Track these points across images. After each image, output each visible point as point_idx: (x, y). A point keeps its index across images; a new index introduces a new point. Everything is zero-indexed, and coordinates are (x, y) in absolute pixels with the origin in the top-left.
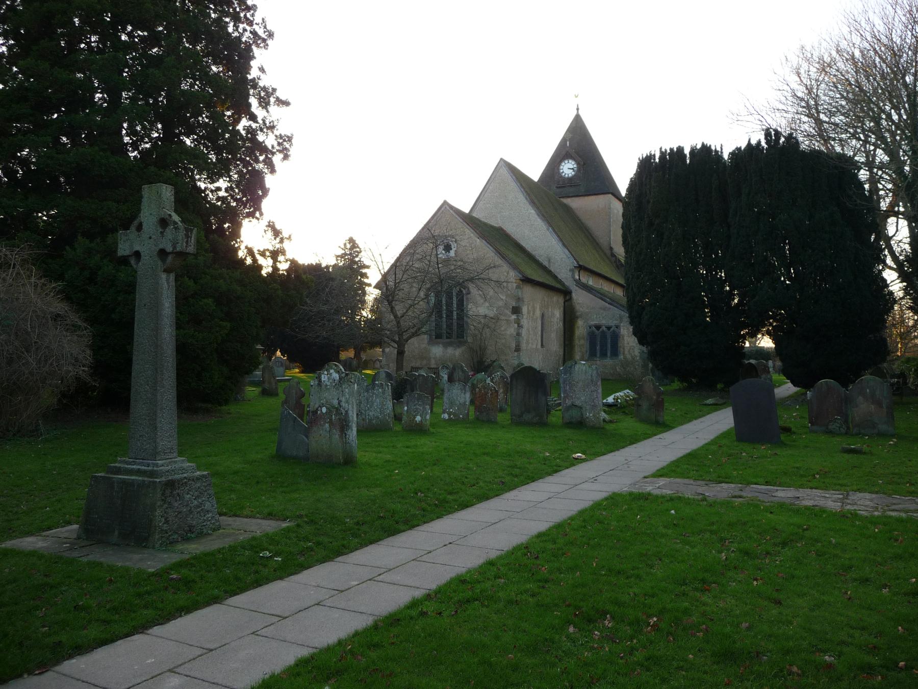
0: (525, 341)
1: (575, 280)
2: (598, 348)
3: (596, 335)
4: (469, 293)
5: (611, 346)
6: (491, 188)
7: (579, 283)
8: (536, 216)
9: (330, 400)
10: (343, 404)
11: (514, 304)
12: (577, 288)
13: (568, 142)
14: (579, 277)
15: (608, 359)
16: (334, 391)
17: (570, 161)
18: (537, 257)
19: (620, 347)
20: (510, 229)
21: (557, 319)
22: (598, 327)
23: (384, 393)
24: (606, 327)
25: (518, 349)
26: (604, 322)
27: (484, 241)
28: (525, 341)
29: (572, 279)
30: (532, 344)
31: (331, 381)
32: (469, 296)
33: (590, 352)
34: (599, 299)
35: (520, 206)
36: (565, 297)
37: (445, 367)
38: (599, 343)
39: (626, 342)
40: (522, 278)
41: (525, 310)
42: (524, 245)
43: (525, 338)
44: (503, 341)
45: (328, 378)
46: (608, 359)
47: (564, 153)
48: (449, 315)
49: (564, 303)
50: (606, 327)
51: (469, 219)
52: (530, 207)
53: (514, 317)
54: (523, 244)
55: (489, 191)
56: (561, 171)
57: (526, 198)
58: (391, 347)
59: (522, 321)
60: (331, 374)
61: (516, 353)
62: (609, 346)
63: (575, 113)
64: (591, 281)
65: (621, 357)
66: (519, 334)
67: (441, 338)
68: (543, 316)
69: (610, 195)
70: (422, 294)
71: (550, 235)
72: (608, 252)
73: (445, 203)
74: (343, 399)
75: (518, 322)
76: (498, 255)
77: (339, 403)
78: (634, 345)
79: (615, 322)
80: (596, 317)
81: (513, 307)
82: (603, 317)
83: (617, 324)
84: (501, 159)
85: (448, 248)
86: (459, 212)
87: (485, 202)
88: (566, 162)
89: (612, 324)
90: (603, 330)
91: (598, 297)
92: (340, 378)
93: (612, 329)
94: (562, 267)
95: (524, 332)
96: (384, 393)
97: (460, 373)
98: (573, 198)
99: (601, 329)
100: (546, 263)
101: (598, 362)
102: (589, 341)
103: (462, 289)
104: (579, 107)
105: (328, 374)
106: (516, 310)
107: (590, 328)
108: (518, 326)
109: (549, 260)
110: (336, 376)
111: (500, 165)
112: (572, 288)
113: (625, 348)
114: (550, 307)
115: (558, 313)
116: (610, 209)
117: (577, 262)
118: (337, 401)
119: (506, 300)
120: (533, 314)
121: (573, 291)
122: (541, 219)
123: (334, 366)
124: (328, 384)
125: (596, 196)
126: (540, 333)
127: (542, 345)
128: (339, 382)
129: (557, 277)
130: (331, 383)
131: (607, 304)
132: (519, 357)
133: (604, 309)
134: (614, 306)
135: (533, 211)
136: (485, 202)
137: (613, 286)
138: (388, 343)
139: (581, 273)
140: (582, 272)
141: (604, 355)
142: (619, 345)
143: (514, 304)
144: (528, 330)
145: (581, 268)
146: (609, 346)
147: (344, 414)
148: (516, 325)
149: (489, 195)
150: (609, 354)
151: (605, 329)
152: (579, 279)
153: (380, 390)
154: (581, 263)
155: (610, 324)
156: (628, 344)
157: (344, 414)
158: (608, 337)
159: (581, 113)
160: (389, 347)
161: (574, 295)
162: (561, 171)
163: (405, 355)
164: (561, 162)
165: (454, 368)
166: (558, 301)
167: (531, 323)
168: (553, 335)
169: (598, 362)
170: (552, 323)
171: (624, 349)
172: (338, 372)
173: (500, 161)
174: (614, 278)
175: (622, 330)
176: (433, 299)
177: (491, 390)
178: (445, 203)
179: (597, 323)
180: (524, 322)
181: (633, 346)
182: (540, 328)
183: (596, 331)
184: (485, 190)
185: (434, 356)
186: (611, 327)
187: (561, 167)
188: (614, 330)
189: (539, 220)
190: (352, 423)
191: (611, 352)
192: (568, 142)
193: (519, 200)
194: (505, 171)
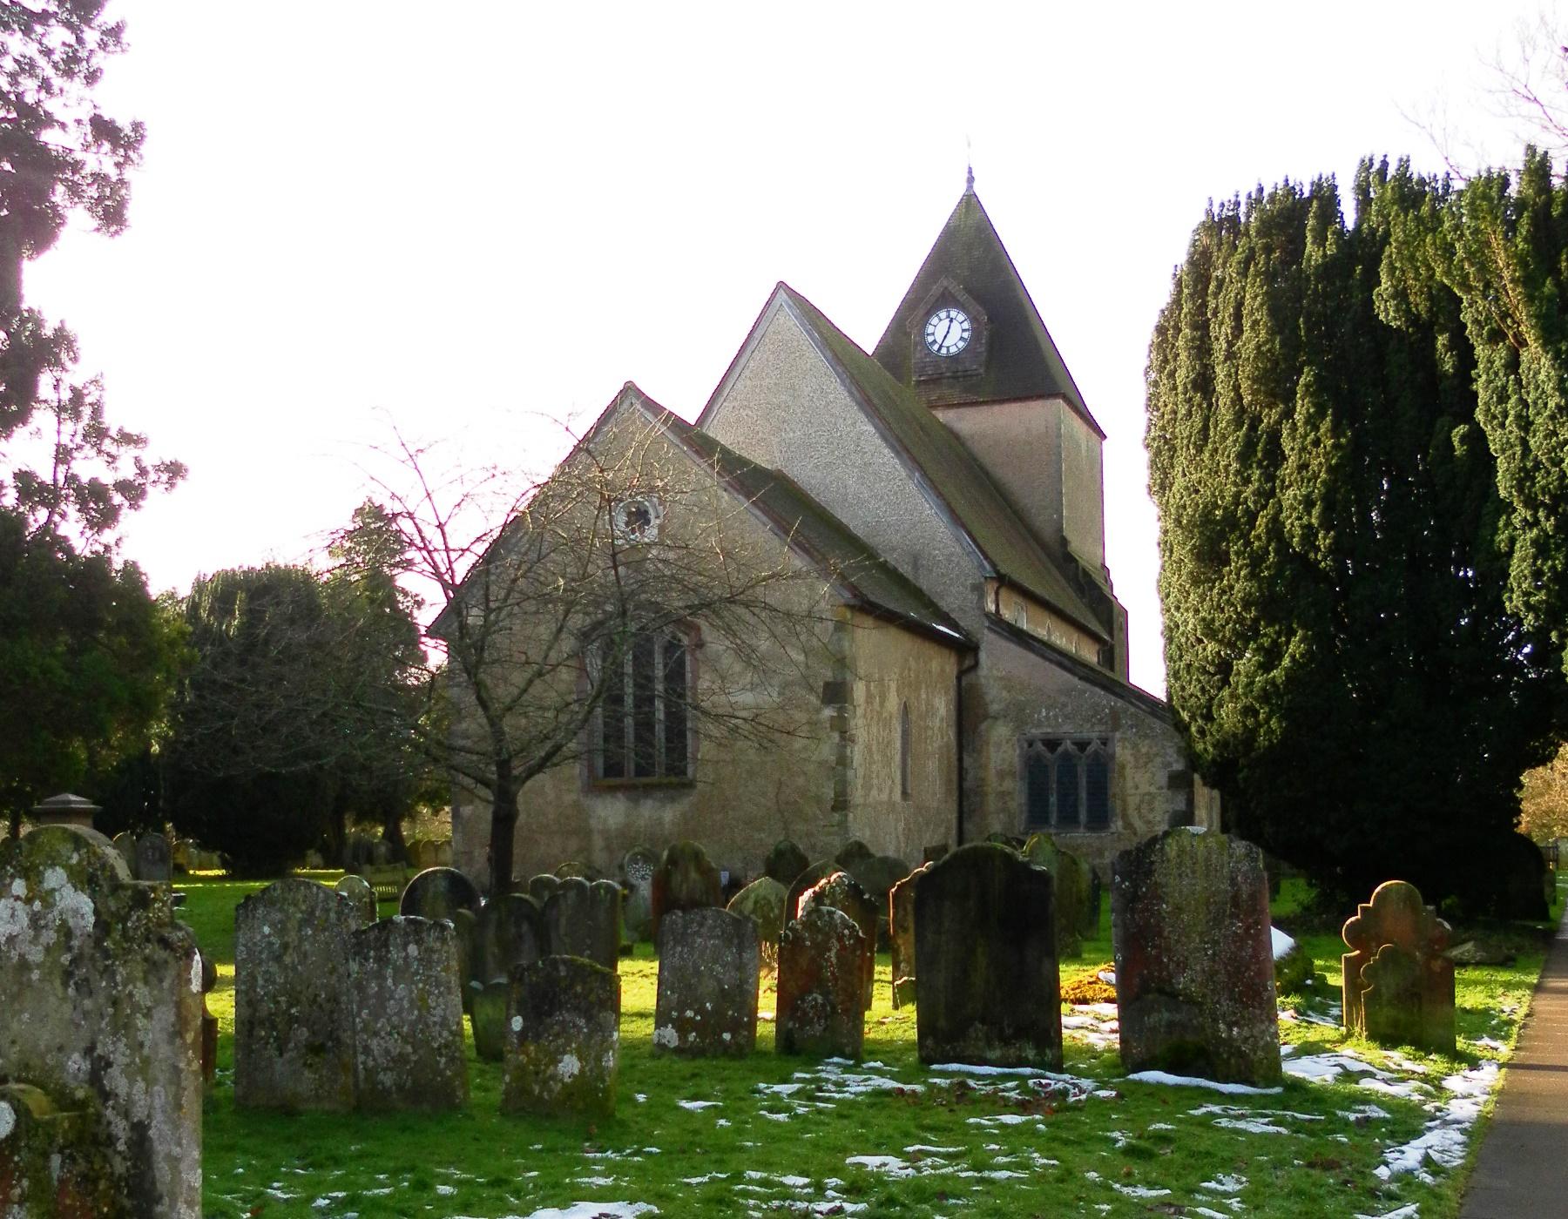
0: (860, 782)
1: (987, 615)
2: (1053, 799)
4: (700, 645)
6: (752, 364)
7: (998, 624)
8: (879, 442)
9: (42, 1056)
10: (117, 1080)
11: (828, 674)
14: (997, 606)
15: (1082, 830)
16: (65, 999)
19: (1114, 795)
20: (805, 473)
21: (942, 720)
22: (1052, 744)
23: (426, 960)
24: (1075, 743)
25: (841, 804)
28: (860, 782)
29: (977, 612)
30: (880, 790)
31: (50, 936)
32: (698, 654)
34: (1053, 667)
36: (960, 662)
37: (648, 857)
38: (1054, 786)
39: (1130, 784)
40: (853, 602)
41: (859, 691)
43: (861, 772)
44: (801, 781)
45: (35, 921)
46: (1082, 830)
48: (645, 700)
49: (959, 679)
51: (694, 438)
52: (862, 416)
53: (828, 712)
54: (843, 516)
55: (747, 372)
56: (930, 339)
57: (851, 393)
58: (477, 801)
59: (852, 723)
60: (48, 898)
63: (960, 190)
64: (1015, 612)
65: (1117, 825)
66: (843, 761)
67: (620, 773)
68: (905, 710)
70: (567, 644)
73: (630, 391)
74: (119, 1054)
75: (841, 726)
77: (95, 1078)
78: (1153, 789)
81: (827, 685)
82: (1066, 717)
85: (639, 517)
86: (678, 425)
87: (736, 404)
91: (1051, 661)
92: (104, 928)
94: (951, 579)
95: (857, 754)
96: (426, 960)
97: (693, 875)
99: (1060, 749)
100: (905, 569)
103: (680, 635)
105: (28, 901)
106: (836, 693)
107: (1030, 745)
110: (78, 905)
111: (777, 302)
113: (1130, 799)
116: (1059, 436)
117: (994, 565)
118: (86, 1066)
119: (807, 667)
120: (882, 704)
122: (892, 447)
123: (65, 848)
124: (36, 955)
126: (898, 758)
127: (905, 794)
128: (98, 943)
130: (48, 949)
132: (843, 825)
135: (871, 429)
136: (736, 404)
137: (1075, 636)
138: (471, 791)
139: (1000, 598)
140: (1004, 593)
141: (1069, 818)
142: (1110, 793)
143: (829, 674)
144: (868, 748)
145: (1004, 582)
146: (1083, 795)
147: (121, 1147)
148: (836, 736)
149: (749, 382)
153: (413, 950)
154: (1004, 569)
155: (1085, 735)
156: (1137, 788)
157: (121, 1147)
158: (1079, 769)
159: (978, 188)
160: (471, 802)
161: (983, 656)
163: (518, 824)
164: (929, 313)
165: (672, 860)
166: (943, 671)
170: (930, 733)
171: (1124, 801)
172: (89, 878)
173: (774, 294)
174: (1076, 615)
176: (595, 665)
177: (840, 938)
178: (630, 391)
179: (1049, 730)
180: (859, 725)
181: (1149, 794)
182: (898, 744)
183: (1049, 755)
184: (757, 335)
185: (601, 827)
186: (1089, 743)
188: (1096, 753)
189: (886, 451)
190: (173, 1206)
194: (788, 321)
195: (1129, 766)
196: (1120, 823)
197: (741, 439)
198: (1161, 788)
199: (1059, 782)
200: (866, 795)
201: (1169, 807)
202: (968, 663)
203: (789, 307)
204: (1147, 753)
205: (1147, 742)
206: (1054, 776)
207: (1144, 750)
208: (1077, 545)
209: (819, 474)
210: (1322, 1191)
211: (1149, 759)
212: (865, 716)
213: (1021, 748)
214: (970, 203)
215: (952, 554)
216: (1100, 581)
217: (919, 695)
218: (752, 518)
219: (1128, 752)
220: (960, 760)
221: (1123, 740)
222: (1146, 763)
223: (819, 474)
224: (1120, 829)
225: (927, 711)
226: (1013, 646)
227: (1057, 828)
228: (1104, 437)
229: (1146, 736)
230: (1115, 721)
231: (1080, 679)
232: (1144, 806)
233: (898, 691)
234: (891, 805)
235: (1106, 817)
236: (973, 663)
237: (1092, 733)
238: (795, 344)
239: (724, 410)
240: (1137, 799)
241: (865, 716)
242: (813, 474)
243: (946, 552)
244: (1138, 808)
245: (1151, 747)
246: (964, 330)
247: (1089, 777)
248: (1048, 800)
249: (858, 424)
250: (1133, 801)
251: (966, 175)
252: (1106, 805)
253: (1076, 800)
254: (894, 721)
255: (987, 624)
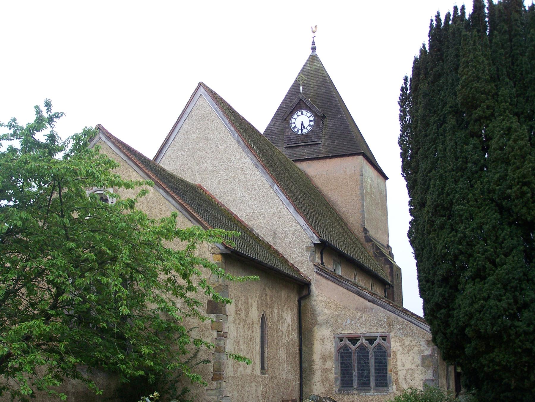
2: (355, 373)
3: (351, 353)
5: (376, 369)
6: (184, 127)
12: (319, 277)
13: (301, 87)
14: (322, 260)
15: (372, 391)
17: (305, 113)
18: (256, 230)
21: (288, 326)
22: (354, 340)
26: (362, 330)
27: (160, 190)
33: (342, 380)
35: (228, 153)
38: (356, 365)
39: (399, 363)
40: (225, 251)
41: (230, 308)
42: (235, 212)
46: (372, 391)
47: (295, 101)
50: (366, 339)
52: (244, 155)
55: (182, 131)
56: (293, 125)
57: (238, 142)
59: (226, 326)
61: (215, 383)
62: (372, 370)
63: (310, 52)
69: (361, 157)
71: (274, 195)
72: (361, 235)
76: (185, 212)
78: (413, 367)
79: (380, 330)
80: (351, 324)
83: (384, 334)
84: (201, 84)
87: (175, 148)
88: (300, 113)
89: (377, 334)
90: (362, 344)
91: (352, 292)
93: (376, 343)
98: (310, 162)
99: (358, 343)
101: (356, 396)
102: (339, 361)
104: (316, 45)
107: (341, 341)
108: (219, 335)
109: (275, 234)
112: (311, 278)
114: (276, 305)
115: (289, 317)
120: (247, 315)
121: (313, 282)
125: (342, 159)
126: (258, 348)
127: (263, 367)
129: (287, 261)
131: (367, 301)
133: (364, 310)
134: (378, 305)
135: (248, 161)
141: (364, 385)
146: (372, 370)
149: (183, 137)
150: (373, 384)
151: (365, 342)
152: (322, 263)
154: (324, 238)
155: (373, 335)
156: (404, 365)
162: (293, 125)
167: (242, 331)
168: (282, 353)
169: (356, 396)
170: (280, 333)
171: (397, 374)
175: (392, 343)
179: (352, 332)
182: (258, 340)
183: (351, 346)
184: (188, 111)
186: (375, 340)
187: (293, 121)
188: (379, 343)
189: (258, 173)
191: (376, 380)
192: (301, 87)
193: (228, 144)
194: (206, 102)
195: (399, 353)
196: (394, 387)
197: (178, 168)
198: (418, 366)
199: (359, 363)
200: (236, 371)
201: (422, 377)
202: (304, 293)
203: (206, 96)
204: (409, 345)
205: (409, 338)
206: (355, 358)
207: (407, 343)
208: (372, 233)
209: (221, 187)
210: (507, 155)
211: (410, 349)
212: (234, 322)
213: (336, 342)
214: (313, 58)
215: (295, 231)
216: (385, 252)
217: (273, 310)
218: (167, 202)
219: (398, 344)
220: (300, 350)
221: (395, 337)
222: (409, 351)
223: (221, 187)
224: (395, 390)
225: (278, 321)
226: (330, 283)
227: (357, 390)
228: (386, 178)
229: (409, 335)
230: (390, 324)
231: (369, 301)
232: (408, 376)
233: (258, 308)
234: (253, 377)
235: (387, 383)
236: (307, 293)
237: (377, 331)
238: (208, 115)
239: (169, 152)
240: (404, 372)
241: (234, 322)
242: (217, 186)
243: (292, 229)
244: (405, 378)
245: (411, 341)
246: (310, 121)
247: (376, 359)
248: (352, 374)
249: (243, 158)
250: (401, 374)
251: (311, 46)
252: (386, 376)
253: (369, 373)
254: (255, 325)
255: (315, 270)
